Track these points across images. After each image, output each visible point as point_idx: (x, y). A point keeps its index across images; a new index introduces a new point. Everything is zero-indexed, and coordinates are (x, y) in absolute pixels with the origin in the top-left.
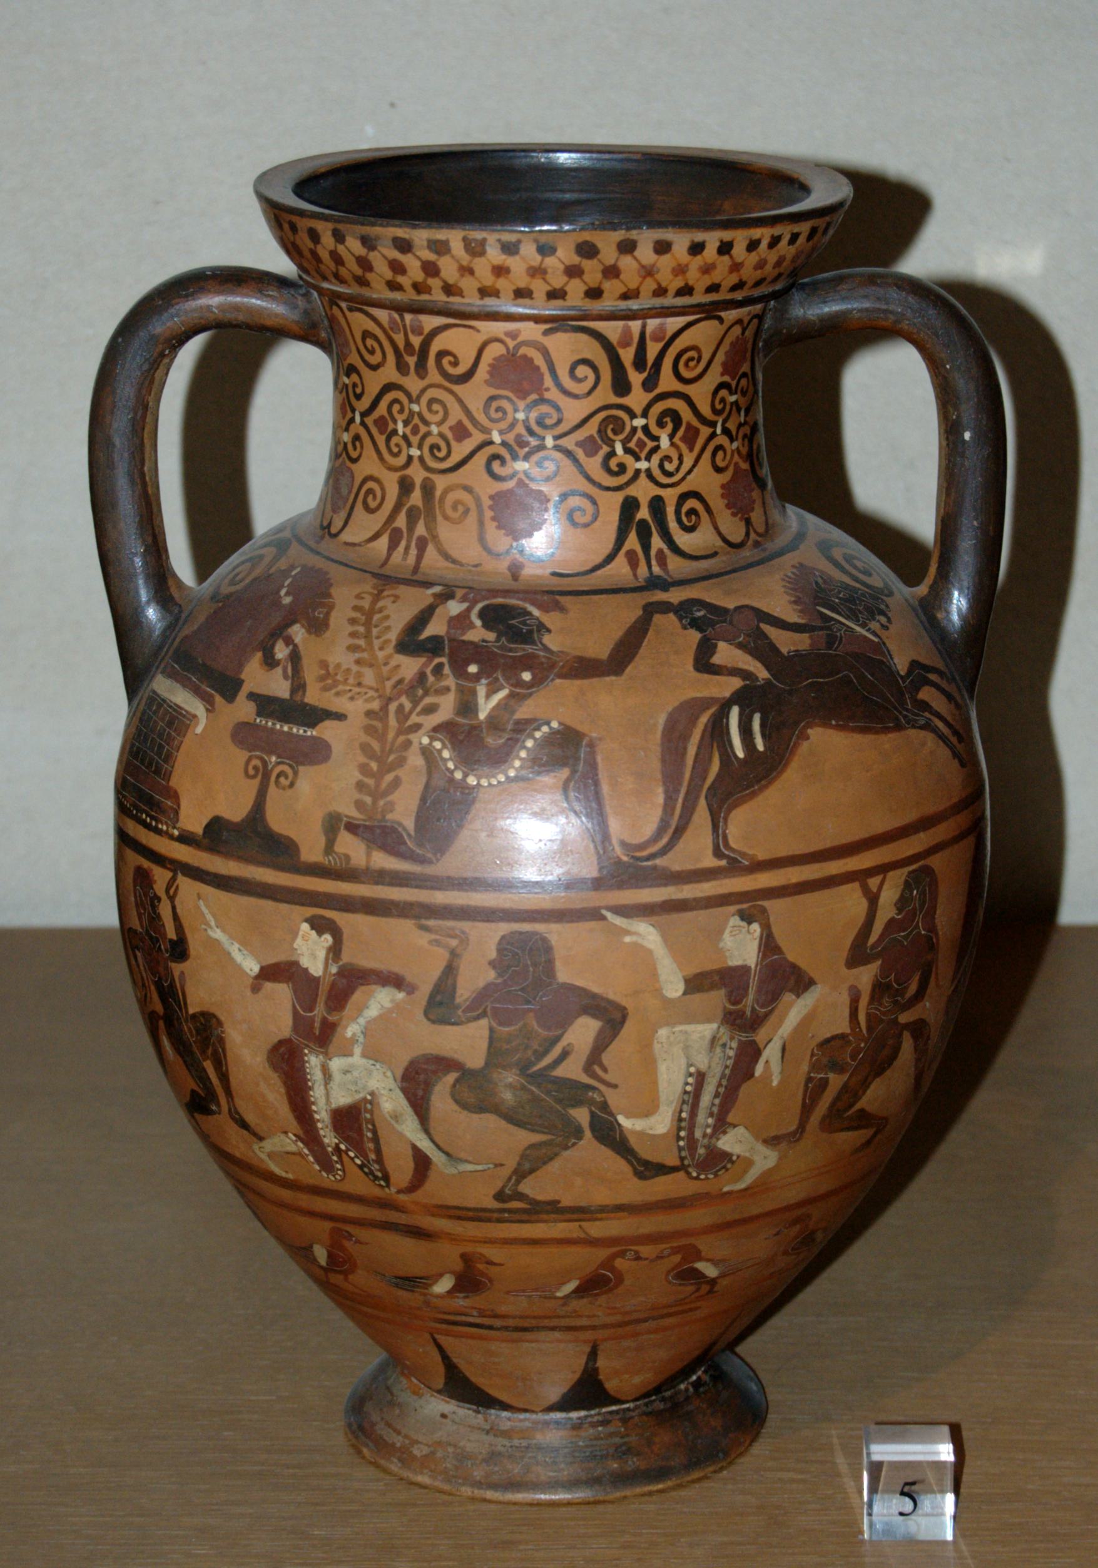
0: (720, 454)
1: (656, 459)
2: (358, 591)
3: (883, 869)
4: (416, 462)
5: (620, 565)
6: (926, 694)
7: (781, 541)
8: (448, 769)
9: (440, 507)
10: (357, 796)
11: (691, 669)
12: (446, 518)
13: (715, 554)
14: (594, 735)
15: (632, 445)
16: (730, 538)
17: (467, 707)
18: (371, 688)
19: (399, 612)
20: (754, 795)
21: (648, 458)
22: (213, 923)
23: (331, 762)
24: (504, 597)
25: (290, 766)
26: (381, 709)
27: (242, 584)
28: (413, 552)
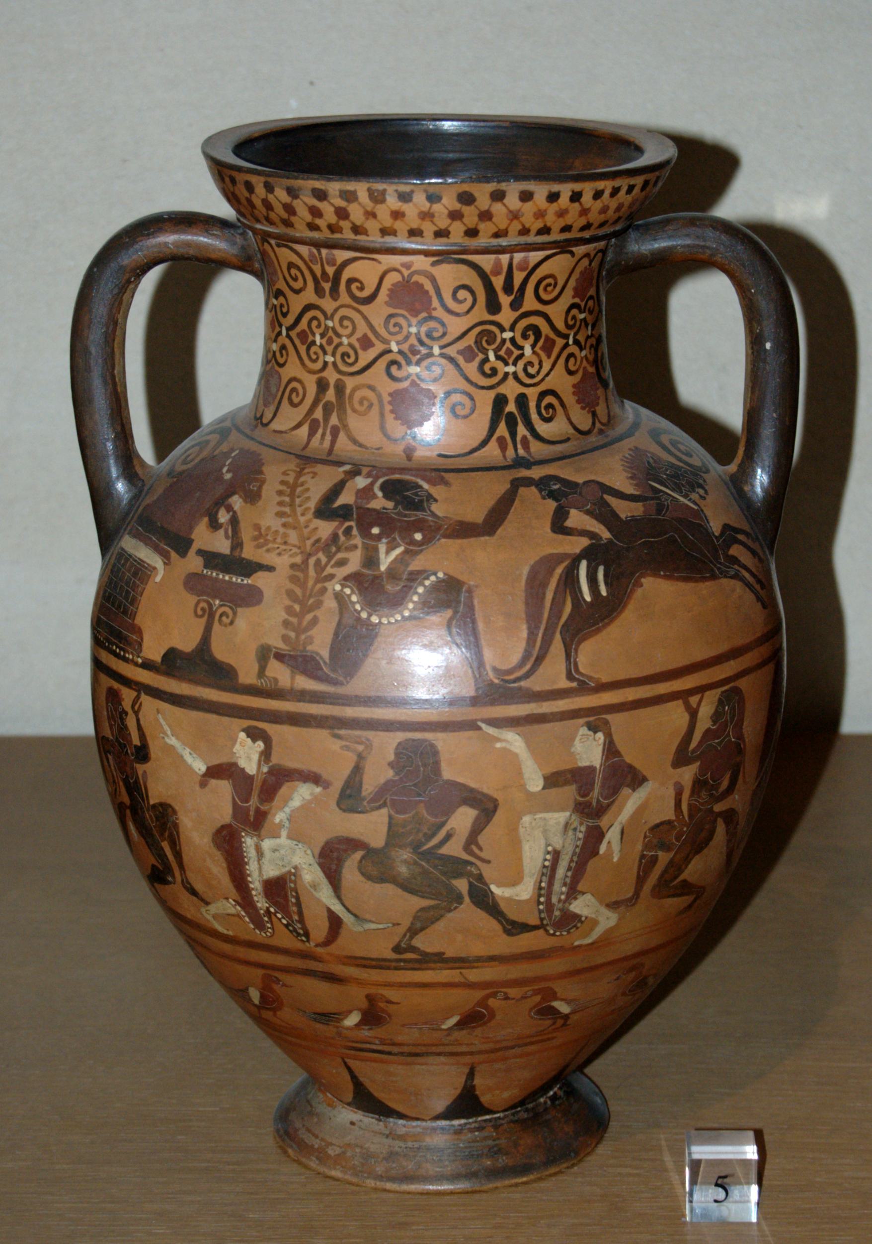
0: (572, 360)
1: (521, 364)
2: (284, 469)
3: (701, 690)
4: (330, 366)
5: (493, 449)
6: (735, 551)
7: (620, 429)
8: (356, 610)
9: (349, 403)
10: (284, 631)
11: (549, 531)
12: (354, 411)
13: (568, 440)
14: (472, 583)
15: (502, 353)
16: (579, 427)
17: (371, 561)
18: (295, 546)
19: (317, 486)
20: (599, 630)
21: (515, 364)
22: (169, 733)
23: (263, 605)
24: (401, 474)
25: (231, 608)
26: (303, 563)
27: (192, 464)
28: (328, 438)
